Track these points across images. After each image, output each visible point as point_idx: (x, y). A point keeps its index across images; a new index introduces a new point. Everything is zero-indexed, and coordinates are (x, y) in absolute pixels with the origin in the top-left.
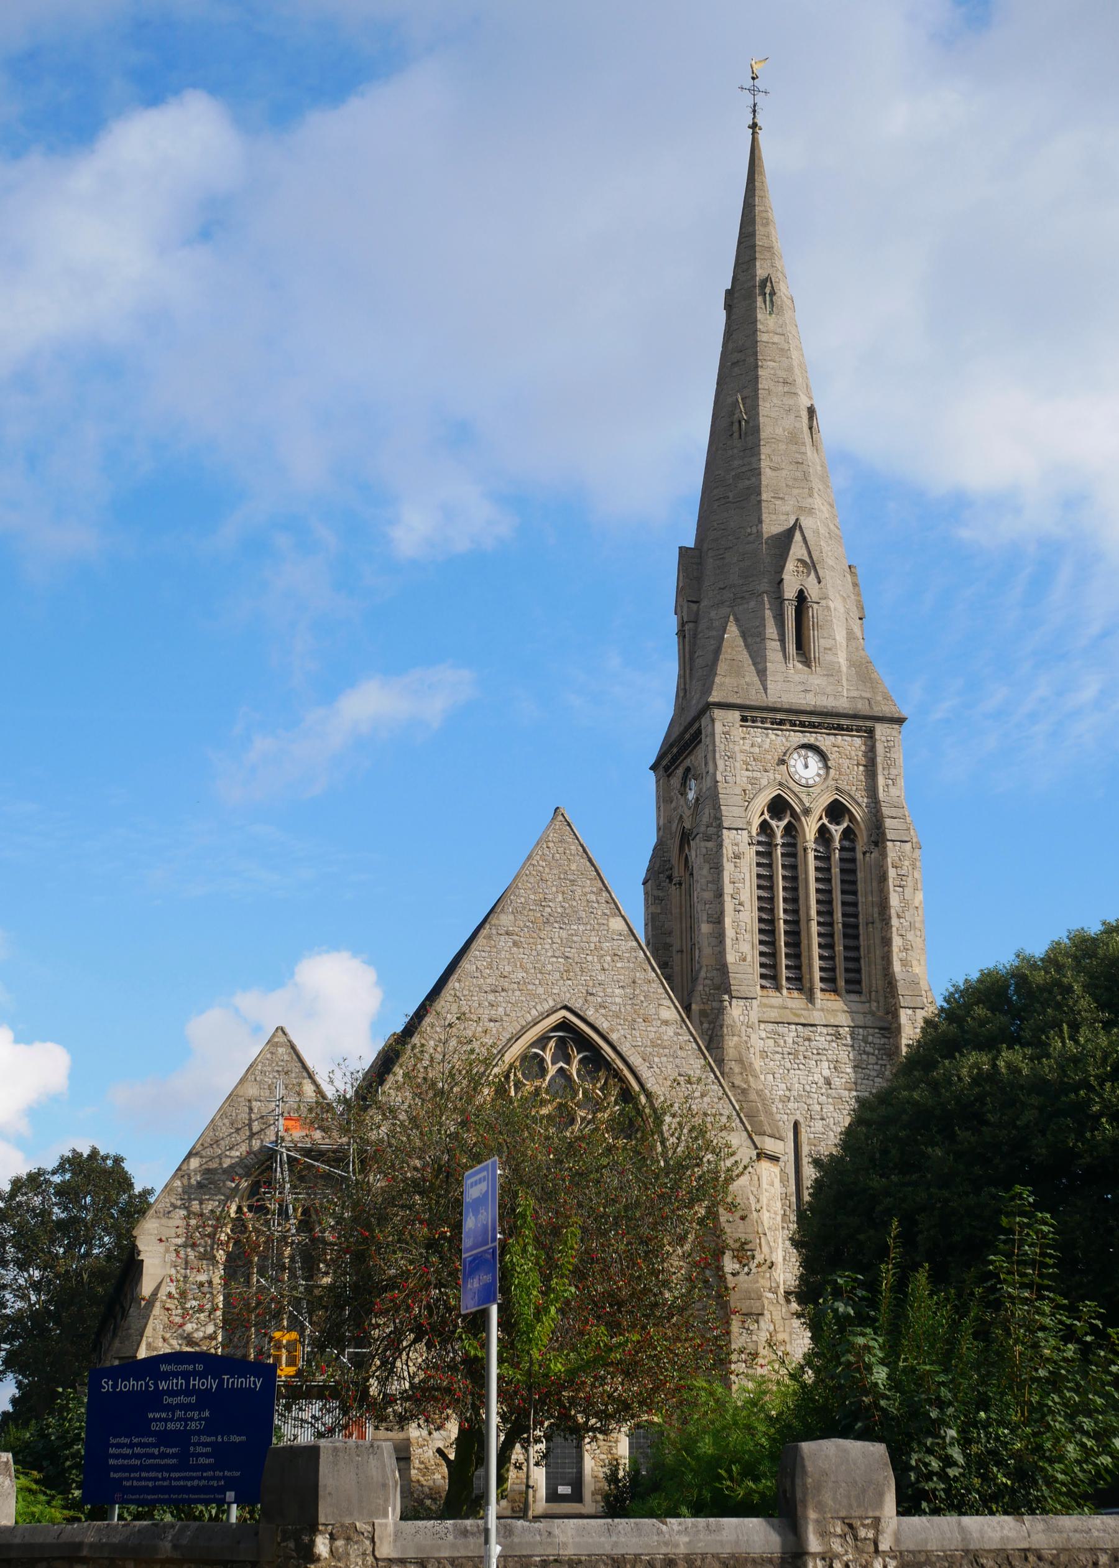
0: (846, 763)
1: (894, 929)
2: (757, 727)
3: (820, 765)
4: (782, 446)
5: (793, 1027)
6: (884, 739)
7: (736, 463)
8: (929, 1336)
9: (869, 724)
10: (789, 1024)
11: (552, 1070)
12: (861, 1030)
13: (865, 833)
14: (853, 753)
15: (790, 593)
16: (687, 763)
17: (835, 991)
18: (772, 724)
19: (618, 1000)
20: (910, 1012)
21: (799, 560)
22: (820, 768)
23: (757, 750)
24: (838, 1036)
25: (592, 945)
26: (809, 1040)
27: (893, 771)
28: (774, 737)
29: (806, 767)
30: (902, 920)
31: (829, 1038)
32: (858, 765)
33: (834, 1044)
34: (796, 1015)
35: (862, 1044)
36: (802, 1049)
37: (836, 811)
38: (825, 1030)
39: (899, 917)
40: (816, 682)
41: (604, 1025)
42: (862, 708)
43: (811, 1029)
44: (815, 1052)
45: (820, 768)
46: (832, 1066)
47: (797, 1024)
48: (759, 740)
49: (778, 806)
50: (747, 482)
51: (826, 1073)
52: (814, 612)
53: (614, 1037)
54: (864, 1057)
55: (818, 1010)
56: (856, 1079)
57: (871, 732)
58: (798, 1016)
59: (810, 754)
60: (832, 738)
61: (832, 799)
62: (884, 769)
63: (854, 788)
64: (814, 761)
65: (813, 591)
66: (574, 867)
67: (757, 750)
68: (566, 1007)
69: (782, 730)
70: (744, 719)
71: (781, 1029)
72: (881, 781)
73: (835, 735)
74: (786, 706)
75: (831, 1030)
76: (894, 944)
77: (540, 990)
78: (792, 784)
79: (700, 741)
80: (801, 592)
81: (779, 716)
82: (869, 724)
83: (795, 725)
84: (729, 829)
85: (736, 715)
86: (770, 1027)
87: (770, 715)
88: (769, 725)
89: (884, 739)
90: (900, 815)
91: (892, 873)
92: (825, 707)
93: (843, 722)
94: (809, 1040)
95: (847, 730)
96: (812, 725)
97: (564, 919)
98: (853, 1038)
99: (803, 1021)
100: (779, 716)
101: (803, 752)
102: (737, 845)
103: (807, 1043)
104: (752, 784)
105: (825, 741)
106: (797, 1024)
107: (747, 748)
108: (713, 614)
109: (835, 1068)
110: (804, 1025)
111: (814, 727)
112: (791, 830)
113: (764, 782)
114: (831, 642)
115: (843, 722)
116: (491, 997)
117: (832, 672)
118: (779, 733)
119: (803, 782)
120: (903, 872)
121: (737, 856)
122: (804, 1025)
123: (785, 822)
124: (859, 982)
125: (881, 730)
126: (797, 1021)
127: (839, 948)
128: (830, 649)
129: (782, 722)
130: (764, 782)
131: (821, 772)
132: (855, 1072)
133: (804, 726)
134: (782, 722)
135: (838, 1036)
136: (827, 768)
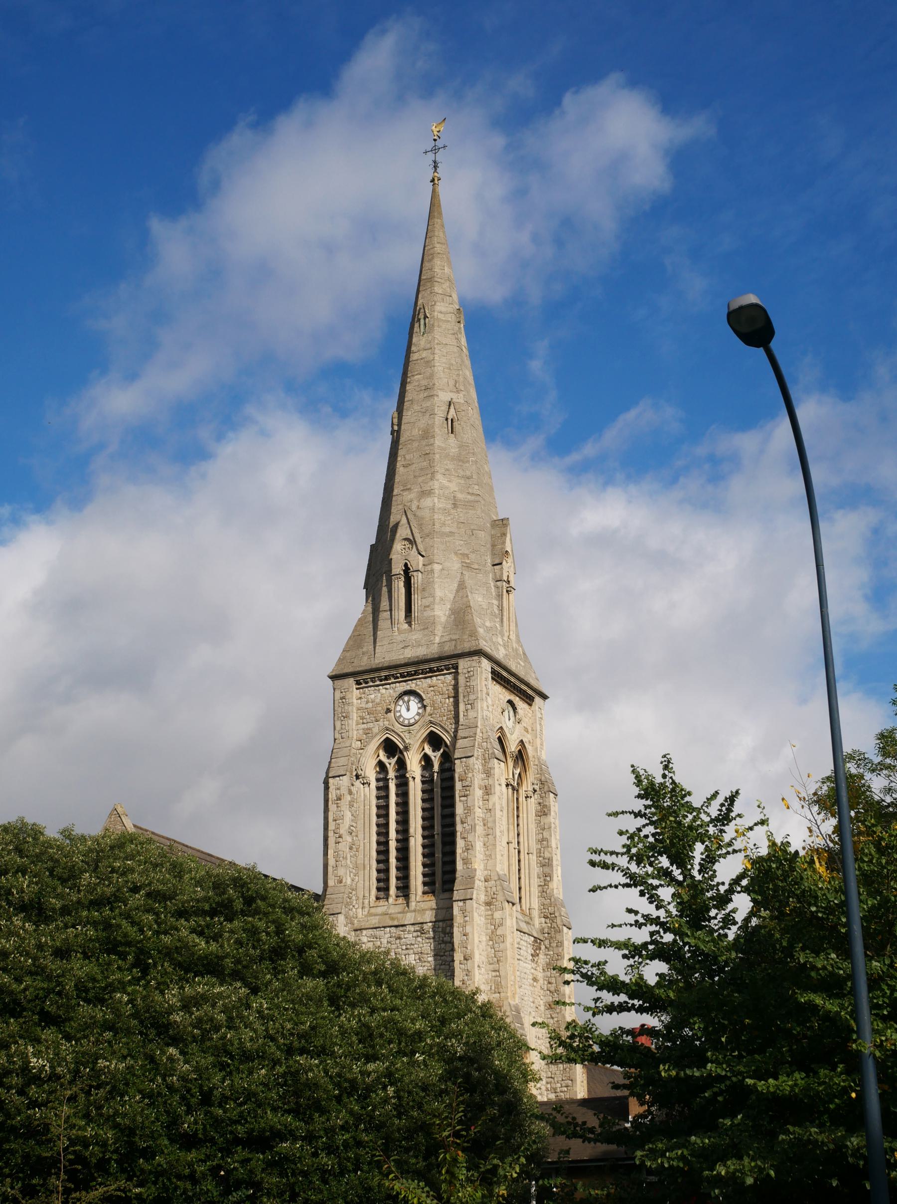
0: (438, 698)
1: (458, 834)
2: (371, 686)
3: (420, 705)
4: (415, 444)
5: (388, 929)
6: (465, 671)
9: (453, 662)
10: (385, 927)
12: (441, 924)
14: (445, 689)
15: (397, 568)
17: (433, 892)
18: (381, 681)
20: (461, 904)
21: (405, 539)
22: (419, 708)
23: (370, 705)
24: (422, 932)
25: (651, 839)
26: (399, 938)
27: (472, 697)
28: (384, 691)
29: (408, 710)
30: (465, 825)
31: (415, 934)
32: (449, 697)
33: (419, 939)
34: (393, 919)
35: (442, 935)
36: (394, 946)
38: (412, 928)
39: (462, 823)
40: (414, 637)
42: (448, 649)
43: (401, 928)
44: (404, 947)
45: (419, 708)
46: (417, 957)
47: (391, 927)
48: (373, 696)
52: (417, 579)
54: (443, 946)
55: (412, 912)
56: (435, 966)
57: (456, 667)
58: (393, 919)
59: (412, 698)
60: (429, 680)
61: (428, 731)
62: (464, 697)
63: (445, 718)
64: (414, 704)
65: (417, 562)
67: (370, 705)
69: (389, 684)
70: (358, 683)
71: (378, 933)
72: (462, 707)
73: (431, 677)
74: (386, 664)
75: (417, 928)
76: (458, 846)
81: (383, 674)
82: (453, 662)
83: (397, 678)
84: (334, 777)
85: (351, 681)
86: (370, 932)
87: (376, 675)
88: (378, 683)
89: (465, 671)
90: (471, 734)
91: (458, 786)
92: (417, 657)
93: (433, 665)
94: (399, 938)
95: (438, 670)
96: (409, 674)
98: (434, 931)
99: (396, 923)
101: (406, 698)
102: (339, 789)
103: (398, 941)
104: (366, 734)
105: (420, 685)
106: (391, 927)
107: (363, 705)
109: (419, 959)
110: (396, 926)
111: (413, 675)
112: (401, 765)
113: (376, 730)
114: (431, 599)
115: (433, 665)
117: (428, 626)
118: (388, 686)
120: (467, 784)
121: (339, 799)
122: (396, 926)
123: (442, 750)
125: (463, 664)
126: (391, 923)
127: (438, 855)
128: (428, 606)
130: (376, 730)
131: (420, 711)
132: (435, 960)
133: (405, 677)
135: (422, 932)
136: (424, 707)
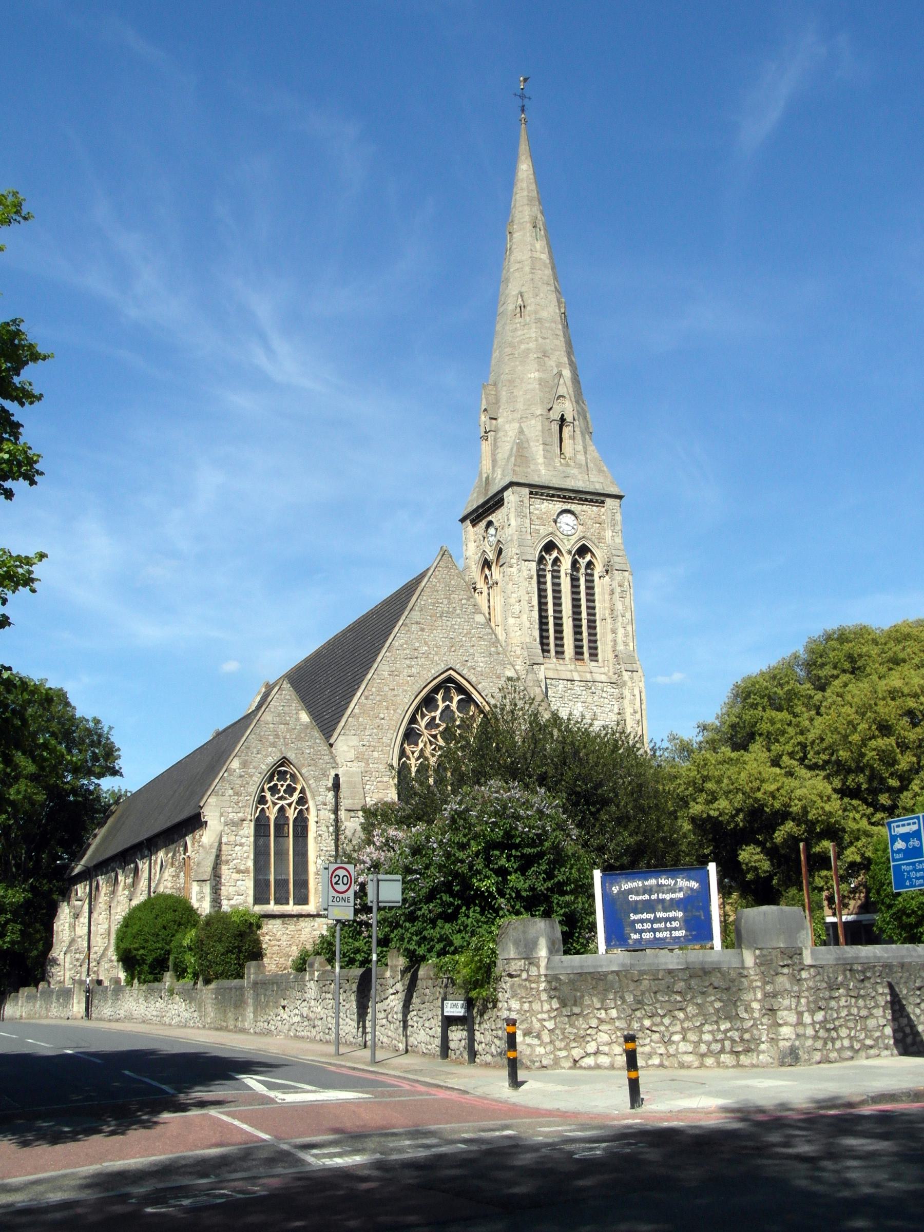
7: (519, 333)
8: (878, 807)
11: (441, 706)
13: (601, 565)
16: (490, 518)
19: (481, 665)
33: (584, 692)
37: (583, 550)
38: (580, 683)
41: (473, 680)
49: (550, 547)
50: (527, 346)
51: (581, 709)
53: (479, 687)
66: (453, 582)
68: (451, 668)
70: (531, 493)
77: (436, 658)
78: (559, 534)
79: (503, 504)
80: (563, 415)
81: (552, 492)
85: (526, 491)
93: (588, 497)
96: (570, 498)
97: (450, 614)
100: (552, 492)
108: (507, 426)
115: (588, 497)
116: (408, 662)
119: (565, 533)
124: (596, 655)
129: (553, 496)
134: (553, 496)
